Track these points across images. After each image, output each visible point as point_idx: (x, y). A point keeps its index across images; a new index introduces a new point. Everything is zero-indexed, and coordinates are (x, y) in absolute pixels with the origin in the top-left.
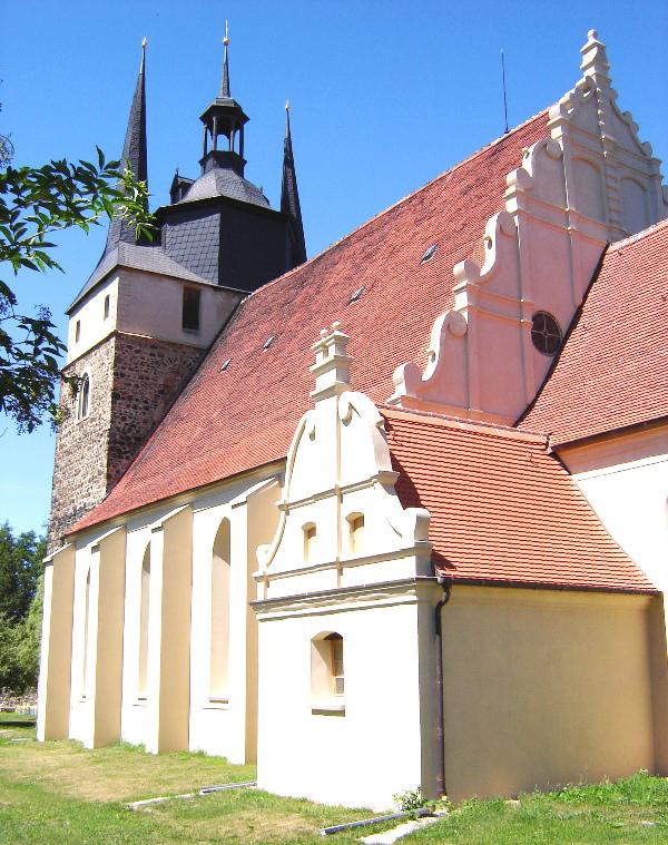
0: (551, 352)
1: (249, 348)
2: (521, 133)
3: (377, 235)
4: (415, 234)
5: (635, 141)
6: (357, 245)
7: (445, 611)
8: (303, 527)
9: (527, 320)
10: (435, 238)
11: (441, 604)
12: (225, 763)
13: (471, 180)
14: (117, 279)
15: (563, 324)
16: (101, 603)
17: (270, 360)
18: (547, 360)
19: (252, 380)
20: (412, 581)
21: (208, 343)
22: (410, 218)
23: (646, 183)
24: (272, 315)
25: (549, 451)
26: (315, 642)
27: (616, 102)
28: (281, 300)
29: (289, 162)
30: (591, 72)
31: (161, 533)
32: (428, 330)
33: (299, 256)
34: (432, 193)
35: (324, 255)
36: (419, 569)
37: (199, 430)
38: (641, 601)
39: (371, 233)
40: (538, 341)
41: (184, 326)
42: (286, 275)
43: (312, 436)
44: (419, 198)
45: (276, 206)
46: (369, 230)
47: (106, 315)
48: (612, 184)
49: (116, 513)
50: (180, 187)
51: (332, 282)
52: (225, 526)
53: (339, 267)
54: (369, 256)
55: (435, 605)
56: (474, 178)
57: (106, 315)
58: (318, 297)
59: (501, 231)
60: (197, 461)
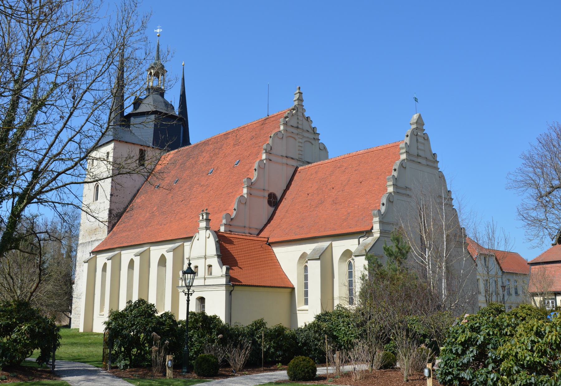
0: (274, 206)
4: (233, 151)
5: (310, 127)
6: (211, 146)
7: (232, 292)
9: (266, 195)
11: (232, 291)
12: (78, 331)
15: (279, 197)
18: (272, 209)
20: (224, 285)
25: (268, 244)
26: (197, 299)
27: (305, 113)
33: (186, 142)
36: (226, 282)
38: (289, 290)
39: (217, 143)
40: (270, 203)
43: (198, 240)
45: (177, 112)
50: (137, 103)
53: (204, 154)
55: (230, 291)
59: (259, 166)
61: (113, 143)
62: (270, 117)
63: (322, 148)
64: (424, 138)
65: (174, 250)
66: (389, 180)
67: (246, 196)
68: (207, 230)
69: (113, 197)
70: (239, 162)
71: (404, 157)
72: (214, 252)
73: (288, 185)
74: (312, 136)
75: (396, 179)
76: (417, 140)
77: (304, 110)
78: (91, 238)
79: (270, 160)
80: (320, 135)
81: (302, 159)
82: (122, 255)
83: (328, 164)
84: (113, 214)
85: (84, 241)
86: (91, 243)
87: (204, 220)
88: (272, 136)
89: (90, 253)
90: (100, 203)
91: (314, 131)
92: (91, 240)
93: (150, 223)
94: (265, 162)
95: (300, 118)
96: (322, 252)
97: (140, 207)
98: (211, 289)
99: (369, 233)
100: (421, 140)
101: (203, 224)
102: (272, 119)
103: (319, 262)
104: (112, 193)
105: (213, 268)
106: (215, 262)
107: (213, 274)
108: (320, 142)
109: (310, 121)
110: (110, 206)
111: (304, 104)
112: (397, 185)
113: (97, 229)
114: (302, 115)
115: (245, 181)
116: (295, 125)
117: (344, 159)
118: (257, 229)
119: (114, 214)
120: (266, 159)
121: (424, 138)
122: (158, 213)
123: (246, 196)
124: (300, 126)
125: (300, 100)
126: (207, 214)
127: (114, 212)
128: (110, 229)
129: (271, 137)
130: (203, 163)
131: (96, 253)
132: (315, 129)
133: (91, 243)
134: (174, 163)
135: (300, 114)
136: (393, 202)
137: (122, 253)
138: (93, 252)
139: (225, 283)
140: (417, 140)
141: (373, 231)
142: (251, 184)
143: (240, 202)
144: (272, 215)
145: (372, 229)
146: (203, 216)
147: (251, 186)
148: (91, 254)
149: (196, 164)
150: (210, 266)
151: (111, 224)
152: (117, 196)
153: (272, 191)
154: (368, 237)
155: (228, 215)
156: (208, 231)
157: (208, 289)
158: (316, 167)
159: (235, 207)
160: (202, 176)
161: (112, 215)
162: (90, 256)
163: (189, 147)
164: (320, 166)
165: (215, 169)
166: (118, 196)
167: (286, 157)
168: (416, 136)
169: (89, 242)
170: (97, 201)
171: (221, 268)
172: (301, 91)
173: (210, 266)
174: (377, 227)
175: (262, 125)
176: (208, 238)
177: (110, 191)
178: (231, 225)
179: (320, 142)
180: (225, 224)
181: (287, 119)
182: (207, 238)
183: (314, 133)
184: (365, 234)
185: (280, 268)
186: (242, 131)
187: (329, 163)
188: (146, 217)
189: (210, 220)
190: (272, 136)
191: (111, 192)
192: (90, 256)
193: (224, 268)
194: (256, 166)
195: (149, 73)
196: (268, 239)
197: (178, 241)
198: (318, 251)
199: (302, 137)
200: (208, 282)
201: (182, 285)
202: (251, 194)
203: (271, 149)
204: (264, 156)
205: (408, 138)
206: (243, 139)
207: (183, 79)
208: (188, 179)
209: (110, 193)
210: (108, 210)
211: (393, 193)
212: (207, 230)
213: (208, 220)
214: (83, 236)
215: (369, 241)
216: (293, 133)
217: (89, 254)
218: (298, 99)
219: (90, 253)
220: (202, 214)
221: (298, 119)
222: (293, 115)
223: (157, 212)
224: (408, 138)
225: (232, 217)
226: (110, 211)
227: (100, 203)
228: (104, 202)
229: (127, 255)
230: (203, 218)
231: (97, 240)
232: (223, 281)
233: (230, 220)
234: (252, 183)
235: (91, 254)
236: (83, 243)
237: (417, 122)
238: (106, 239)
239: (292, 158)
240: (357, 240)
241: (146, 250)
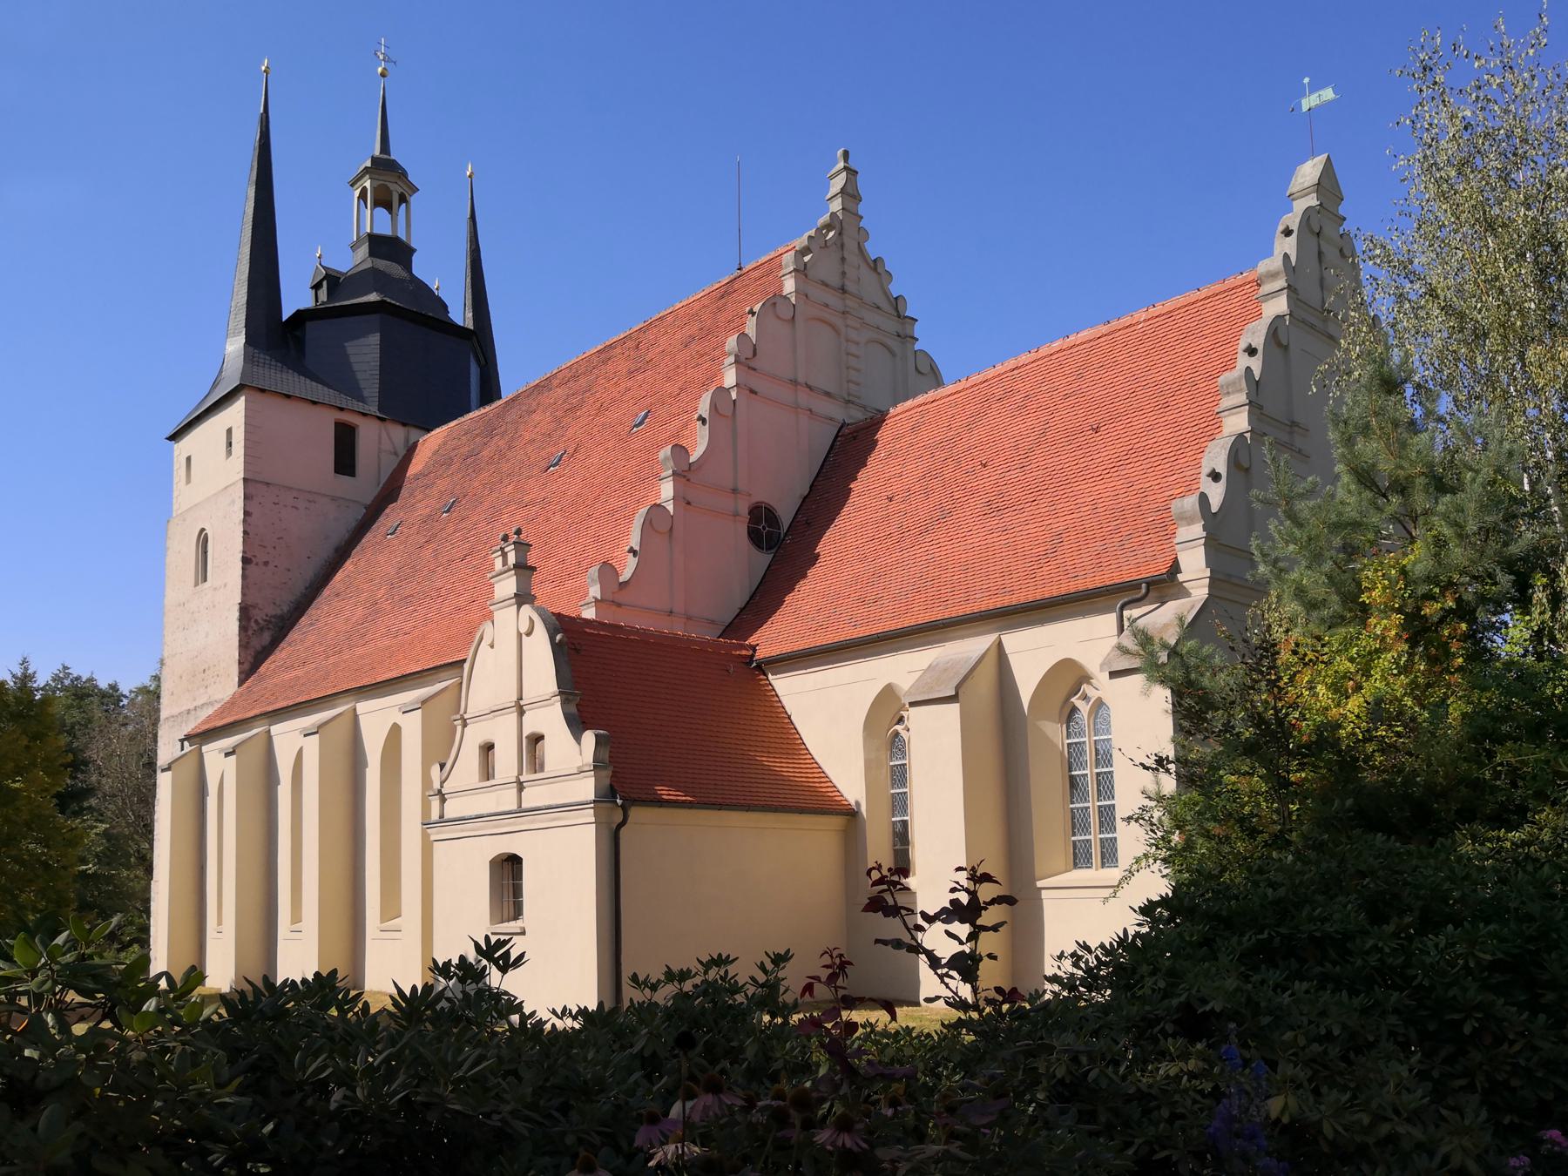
0: (769, 548)
1: (422, 510)
2: (756, 274)
3: (583, 381)
5: (886, 294)
6: (559, 390)
8: (915, 893)
10: (649, 400)
13: (694, 328)
14: (243, 398)
16: (460, 697)
17: (451, 530)
19: (427, 553)
21: (319, 292)
22: (623, 366)
23: (894, 344)
24: (454, 467)
28: (465, 450)
29: (473, 217)
30: (836, 206)
31: (233, 758)
32: (630, 519)
33: (490, 391)
34: (650, 336)
35: (518, 396)
37: (360, 611)
38: (836, 822)
39: (575, 377)
40: (755, 537)
41: (335, 472)
42: (471, 415)
44: (634, 341)
46: (573, 374)
47: (229, 453)
48: (853, 349)
49: (256, 711)
51: (527, 436)
52: (395, 731)
53: (536, 417)
54: (573, 409)
56: (697, 325)
57: (229, 453)
58: (510, 455)
59: (714, 407)
60: (360, 651)
61: (243, 398)
62: (744, 270)
63: (925, 368)
64: (1341, 250)
65: (423, 702)
66: (1229, 389)
67: (670, 507)
68: (519, 605)
69: (251, 567)
70: (646, 416)
71: (1280, 305)
72: (552, 686)
73: (814, 482)
74: (891, 325)
75: (1255, 387)
76: (1320, 253)
77: (863, 234)
78: (195, 700)
79: (752, 391)
80: (917, 323)
81: (859, 398)
82: (275, 740)
83: (955, 396)
84: (256, 621)
85: (176, 711)
86: (193, 712)
87: (510, 570)
88: (757, 308)
89: (182, 741)
90: (215, 589)
91: (896, 309)
92: (195, 704)
93: (363, 635)
94: (734, 395)
95: (852, 258)
96: (964, 672)
97: (337, 595)
98: (542, 821)
99: (1165, 585)
100: (1331, 254)
101: (507, 586)
102: (756, 274)
103: (954, 708)
104: (248, 556)
105: (547, 744)
106: (550, 719)
107: (547, 768)
108: (917, 347)
109: (883, 274)
110: (244, 594)
111: (861, 209)
112: (1261, 408)
113: (209, 668)
114: (857, 251)
115: (666, 459)
116: (835, 280)
117: (1016, 372)
118: (713, 622)
119: (260, 621)
120: (737, 385)
121: (1341, 250)
122: (390, 604)
123: (670, 507)
124: (850, 286)
125: (849, 195)
126: (522, 547)
127: (259, 615)
128: (246, 666)
129: (753, 313)
130: (532, 441)
131: (197, 739)
132: (900, 300)
133: (193, 712)
134: (443, 461)
135: (850, 244)
136: (1247, 470)
137: (272, 733)
138: (188, 738)
139: (592, 797)
140: (1320, 253)
141: (1181, 577)
142: (687, 469)
143: (648, 524)
144: (763, 579)
145: (1175, 568)
146: (504, 555)
147: (689, 475)
148: (186, 743)
149: (510, 448)
150: (537, 739)
151: (251, 652)
152: (266, 563)
153: (761, 496)
154: (1163, 603)
155: (608, 571)
156: (527, 610)
157: (532, 822)
158: (913, 412)
159: (635, 541)
160: (530, 477)
161: (253, 624)
162: (182, 749)
163: (492, 408)
164: (927, 407)
165: (571, 450)
166: (271, 566)
167: (809, 387)
168: (1315, 239)
169: (189, 712)
170: (207, 585)
171: (578, 739)
172: (852, 165)
173: (537, 739)
174: (1194, 566)
175: (722, 297)
176: (529, 634)
177: (240, 547)
178: (619, 605)
179: (917, 347)
180: (597, 600)
181: (806, 259)
182: (524, 636)
183: (899, 316)
184: (1143, 591)
185: (803, 747)
186: (655, 330)
187: (960, 392)
188: (354, 619)
189: (533, 569)
190: (757, 308)
191: (244, 552)
192: (182, 749)
193: (589, 738)
194: (704, 407)
195: (357, 193)
196: (755, 650)
197: (443, 675)
198: (945, 670)
199: (859, 326)
200: (532, 797)
201: (442, 816)
202: (689, 503)
203: (755, 354)
204: (730, 378)
205: (1293, 238)
206: (658, 350)
207: (473, 217)
208: (486, 493)
209: (241, 555)
210: (237, 607)
211: (1248, 435)
212: (519, 605)
213: (523, 569)
214: (172, 694)
215: (1163, 619)
216: (827, 306)
217: (180, 743)
218: (843, 191)
219: (182, 741)
220: (502, 549)
221: (843, 259)
222: (826, 245)
223: (387, 600)
224: (1293, 238)
225: (621, 579)
226: (245, 611)
227: (215, 589)
228: (225, 586)
229: (289, 738)
230: (505, 563)
231: (211, 704)
232: (586, 788)
233: (616, 587)
234: (690, 464)
235: (186, 743)
236: (173, 717)
237: (1318, 184)
238: (233, 697)
239: (828, 394)
240: (1112, 618)
241: (341, 714)
